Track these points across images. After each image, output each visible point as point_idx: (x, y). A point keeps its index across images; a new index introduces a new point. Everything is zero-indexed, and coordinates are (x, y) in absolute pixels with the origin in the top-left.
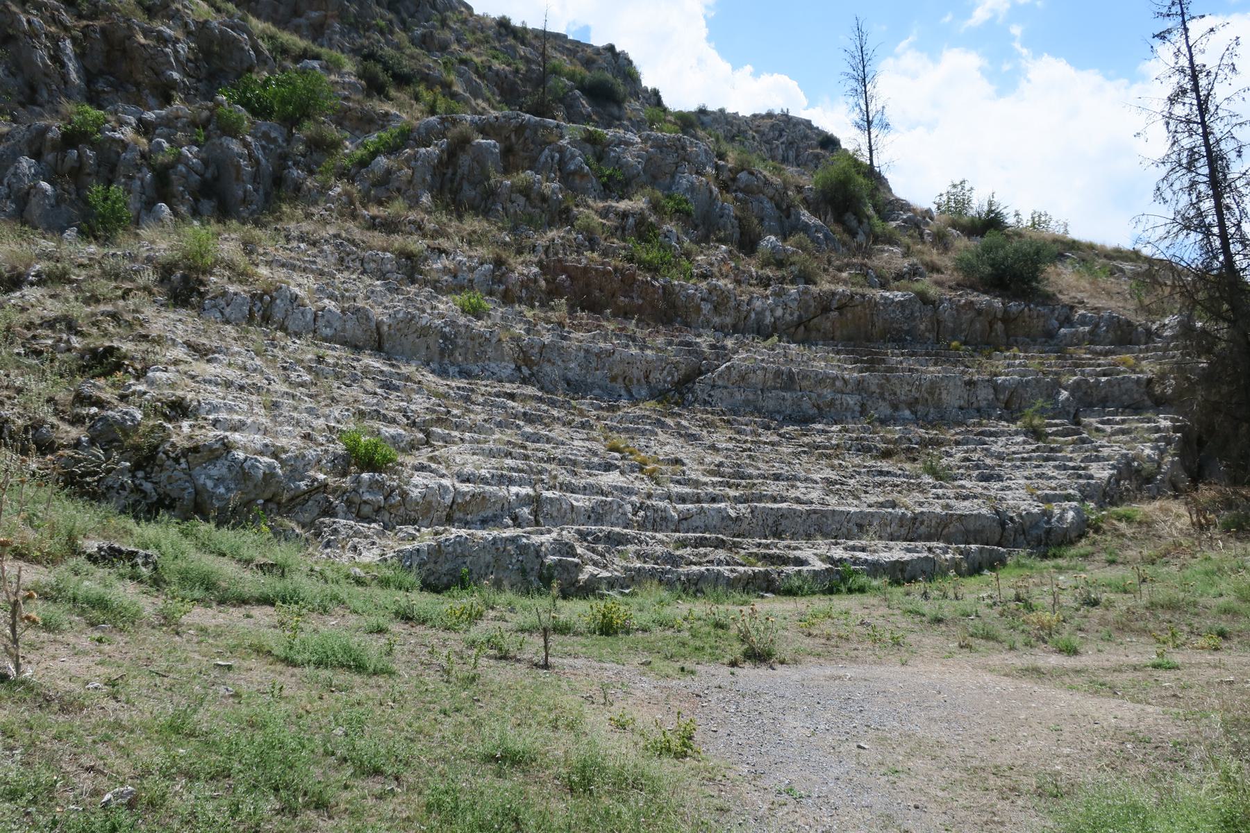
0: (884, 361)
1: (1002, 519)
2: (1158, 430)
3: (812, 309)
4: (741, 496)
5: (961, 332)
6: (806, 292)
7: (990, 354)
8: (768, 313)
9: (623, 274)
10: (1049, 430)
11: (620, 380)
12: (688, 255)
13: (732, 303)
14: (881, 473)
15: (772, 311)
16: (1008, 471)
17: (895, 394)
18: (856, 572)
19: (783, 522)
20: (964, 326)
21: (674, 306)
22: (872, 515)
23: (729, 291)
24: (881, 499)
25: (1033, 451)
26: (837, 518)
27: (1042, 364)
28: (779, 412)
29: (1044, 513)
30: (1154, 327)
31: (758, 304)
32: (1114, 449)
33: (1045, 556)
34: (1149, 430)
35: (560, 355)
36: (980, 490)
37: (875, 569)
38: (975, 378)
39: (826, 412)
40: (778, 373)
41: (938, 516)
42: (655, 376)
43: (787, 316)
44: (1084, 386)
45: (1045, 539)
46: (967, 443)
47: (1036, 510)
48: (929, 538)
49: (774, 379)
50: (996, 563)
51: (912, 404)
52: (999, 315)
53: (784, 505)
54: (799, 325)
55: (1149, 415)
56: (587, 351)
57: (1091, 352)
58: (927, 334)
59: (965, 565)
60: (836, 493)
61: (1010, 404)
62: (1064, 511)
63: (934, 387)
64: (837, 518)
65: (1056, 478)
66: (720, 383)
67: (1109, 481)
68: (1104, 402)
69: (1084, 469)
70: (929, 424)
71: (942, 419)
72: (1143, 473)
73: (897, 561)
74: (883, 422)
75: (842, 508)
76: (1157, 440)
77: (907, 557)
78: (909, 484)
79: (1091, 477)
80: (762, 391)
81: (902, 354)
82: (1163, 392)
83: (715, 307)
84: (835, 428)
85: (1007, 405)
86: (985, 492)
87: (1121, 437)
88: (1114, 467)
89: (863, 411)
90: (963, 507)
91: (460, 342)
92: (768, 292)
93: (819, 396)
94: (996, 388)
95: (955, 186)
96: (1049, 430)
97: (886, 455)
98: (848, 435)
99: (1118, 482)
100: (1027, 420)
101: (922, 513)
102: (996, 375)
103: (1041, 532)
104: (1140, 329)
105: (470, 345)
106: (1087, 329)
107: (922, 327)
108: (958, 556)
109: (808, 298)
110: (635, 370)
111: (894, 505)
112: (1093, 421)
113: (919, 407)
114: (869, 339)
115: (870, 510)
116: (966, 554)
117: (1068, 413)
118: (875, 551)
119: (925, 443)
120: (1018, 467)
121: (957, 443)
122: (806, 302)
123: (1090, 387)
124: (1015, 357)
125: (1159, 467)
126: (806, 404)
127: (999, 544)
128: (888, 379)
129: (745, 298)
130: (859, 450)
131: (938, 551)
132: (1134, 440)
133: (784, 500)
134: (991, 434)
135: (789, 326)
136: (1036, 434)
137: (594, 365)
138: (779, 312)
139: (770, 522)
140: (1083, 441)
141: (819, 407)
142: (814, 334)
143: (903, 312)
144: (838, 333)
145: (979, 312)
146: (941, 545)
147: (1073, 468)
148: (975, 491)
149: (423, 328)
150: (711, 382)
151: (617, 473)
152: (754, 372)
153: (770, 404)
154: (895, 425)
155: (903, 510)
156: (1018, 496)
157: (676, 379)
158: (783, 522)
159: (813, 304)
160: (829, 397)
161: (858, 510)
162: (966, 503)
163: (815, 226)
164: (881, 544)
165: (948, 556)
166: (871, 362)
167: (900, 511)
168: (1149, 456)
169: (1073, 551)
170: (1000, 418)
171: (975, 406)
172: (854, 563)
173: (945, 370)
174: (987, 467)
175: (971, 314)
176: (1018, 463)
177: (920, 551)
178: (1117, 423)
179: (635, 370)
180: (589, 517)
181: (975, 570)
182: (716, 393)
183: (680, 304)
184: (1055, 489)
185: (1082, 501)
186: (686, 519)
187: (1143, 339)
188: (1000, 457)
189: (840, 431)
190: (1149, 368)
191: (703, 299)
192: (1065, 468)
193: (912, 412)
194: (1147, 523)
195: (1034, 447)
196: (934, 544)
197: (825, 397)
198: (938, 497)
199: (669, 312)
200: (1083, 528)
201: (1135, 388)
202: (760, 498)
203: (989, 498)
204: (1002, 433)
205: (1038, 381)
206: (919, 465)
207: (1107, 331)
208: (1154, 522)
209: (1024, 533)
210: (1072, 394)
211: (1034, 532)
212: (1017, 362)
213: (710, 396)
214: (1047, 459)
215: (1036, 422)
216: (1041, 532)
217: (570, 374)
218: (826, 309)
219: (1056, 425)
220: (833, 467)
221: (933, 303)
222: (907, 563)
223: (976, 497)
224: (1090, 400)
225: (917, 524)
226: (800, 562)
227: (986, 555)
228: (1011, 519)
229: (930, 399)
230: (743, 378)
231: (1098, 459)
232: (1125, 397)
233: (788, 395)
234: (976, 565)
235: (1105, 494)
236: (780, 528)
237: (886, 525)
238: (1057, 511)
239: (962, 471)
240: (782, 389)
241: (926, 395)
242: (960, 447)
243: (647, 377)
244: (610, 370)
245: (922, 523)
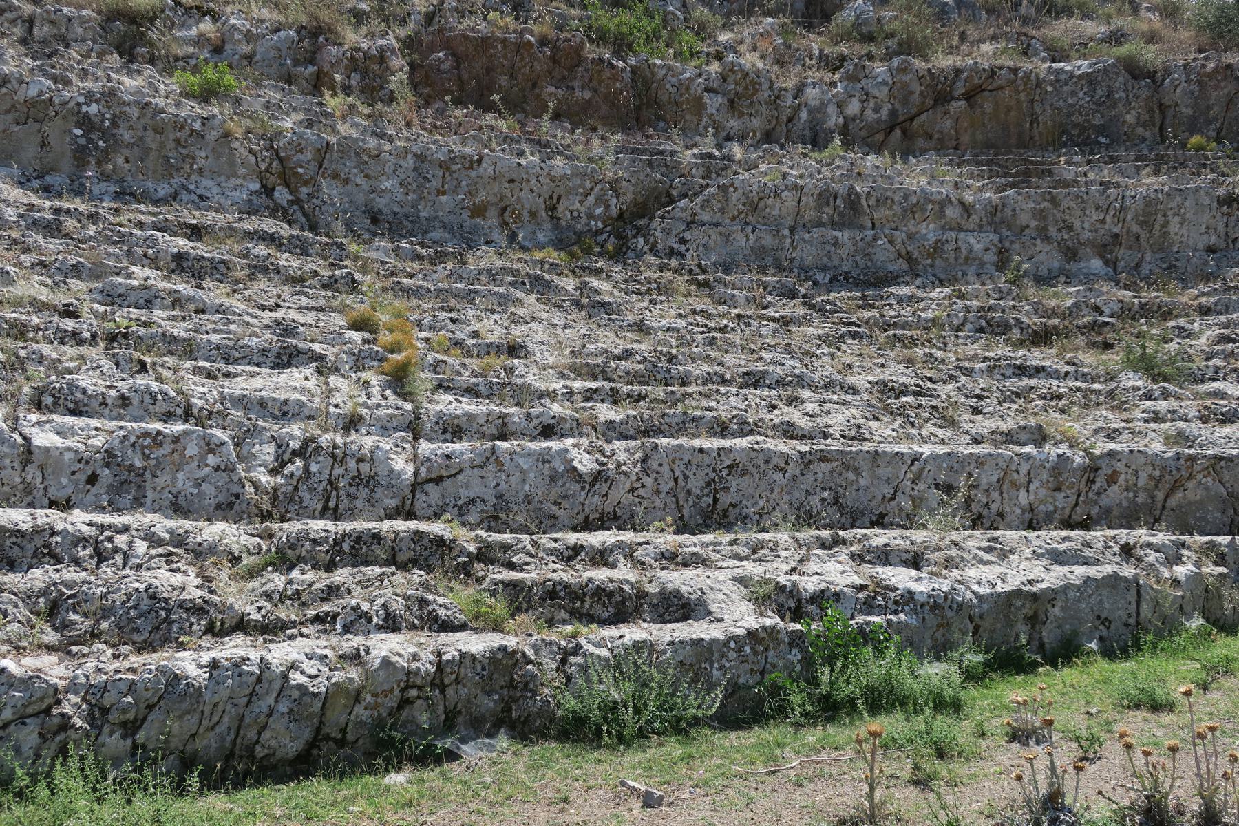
3: (916, 98)
4: (626, 421)
5: (1209, 122)
8: (832, 109)
9: (555, 49)
11: (492, 214)
12: (701, 31)
13: (764, 94)
14: (1021, 370)
15: (840, 106)
17: (1070, 228)
18: (866, 636)
21: (653, 102)
22: (979, 461)
26: (884, 472)
28: (824, 269)
31: (812, 94)
35: (361, 164)
39: (920, 266)
40: (826, 197)
41: (1154, 460)
42: (569, 207)
43: (869, 112)
48: (1129, 520)
49: (818, 208)
51: (1106, 248)
53: (743, 442)
54: (891, 129)
56: (420, 158)
58: (1140, 131)
63: (1151, 208)
64: (884, 472)
66: (706, 217)
70: (1134, 277)
71: (1174, 270)
73: (1017, 593)
75: (903, 448)
77: (1052, 577)
78: (1087, 393)
80: (792, 230)
83: (731, 102)
89: (1002, 264)
91: (127, 135)
92: (837, 76)
93: (911, 236)
97: (1041, 338)
98: (961, 303)
101: (1111, 454)
105: (152, 141)
107: (1130, 118)
108: (1210, 569)
111: (1040, 437)
113: (1122, 252)
114: (1025, 143)
115: (976, 450)
118: (949, 563)
119: (1128, 314)
121: (1204, 311)
122: (905, 85)
126: (883, 254)
128: (1054, 201)
129: (791, 83)
130: (982, 330)
133: (746, 429)
135: (872, 130)
137: (436, 183)
138: (853, 107)
139: (696, 483)
141: (909, 258)
142: (920, 142)
144: (965, 139)
146: (1161, 538)
149: (31, 103)
150: (687, 216)
151: (309, 370)
153: (808, 254)
154: (1068, 283)
155: (1064, 448)
157: (614, 211)
158: (734, 483)
159: (917, 88)
160: (932, 238)
161: (940, 450)
164: (975, 540)
165: (1181, 571)
167: (1052, 452)
172: (869, 606)
177: (1100, 555)
179: (525, 195)
180: (93, 479)
183: (665, 98)
186: (438, 480)
189: (949, 297)
193: (1106, 263)
196: (1142, 534)
197: (924, 238)
198: (1157, 418)
199: (642, 108)
202: (684, 426)
206: (1114, 358)
213: (682, 241)
217: (381, 203)
220: (910, 362)
221: (1152, 75)
222: (1051, 596)
225: (1100, 482)
226: (678, 607)
230: (754, 207)
233: (844, 236)
236: (725, 500)
237: (1015, 486)
239: (1218, 362)
240: (833, 225)
241: (1135, 228)
242: (1211, 319)
243: (554, 208)
244: (471, 193)
245: (1112, 479)
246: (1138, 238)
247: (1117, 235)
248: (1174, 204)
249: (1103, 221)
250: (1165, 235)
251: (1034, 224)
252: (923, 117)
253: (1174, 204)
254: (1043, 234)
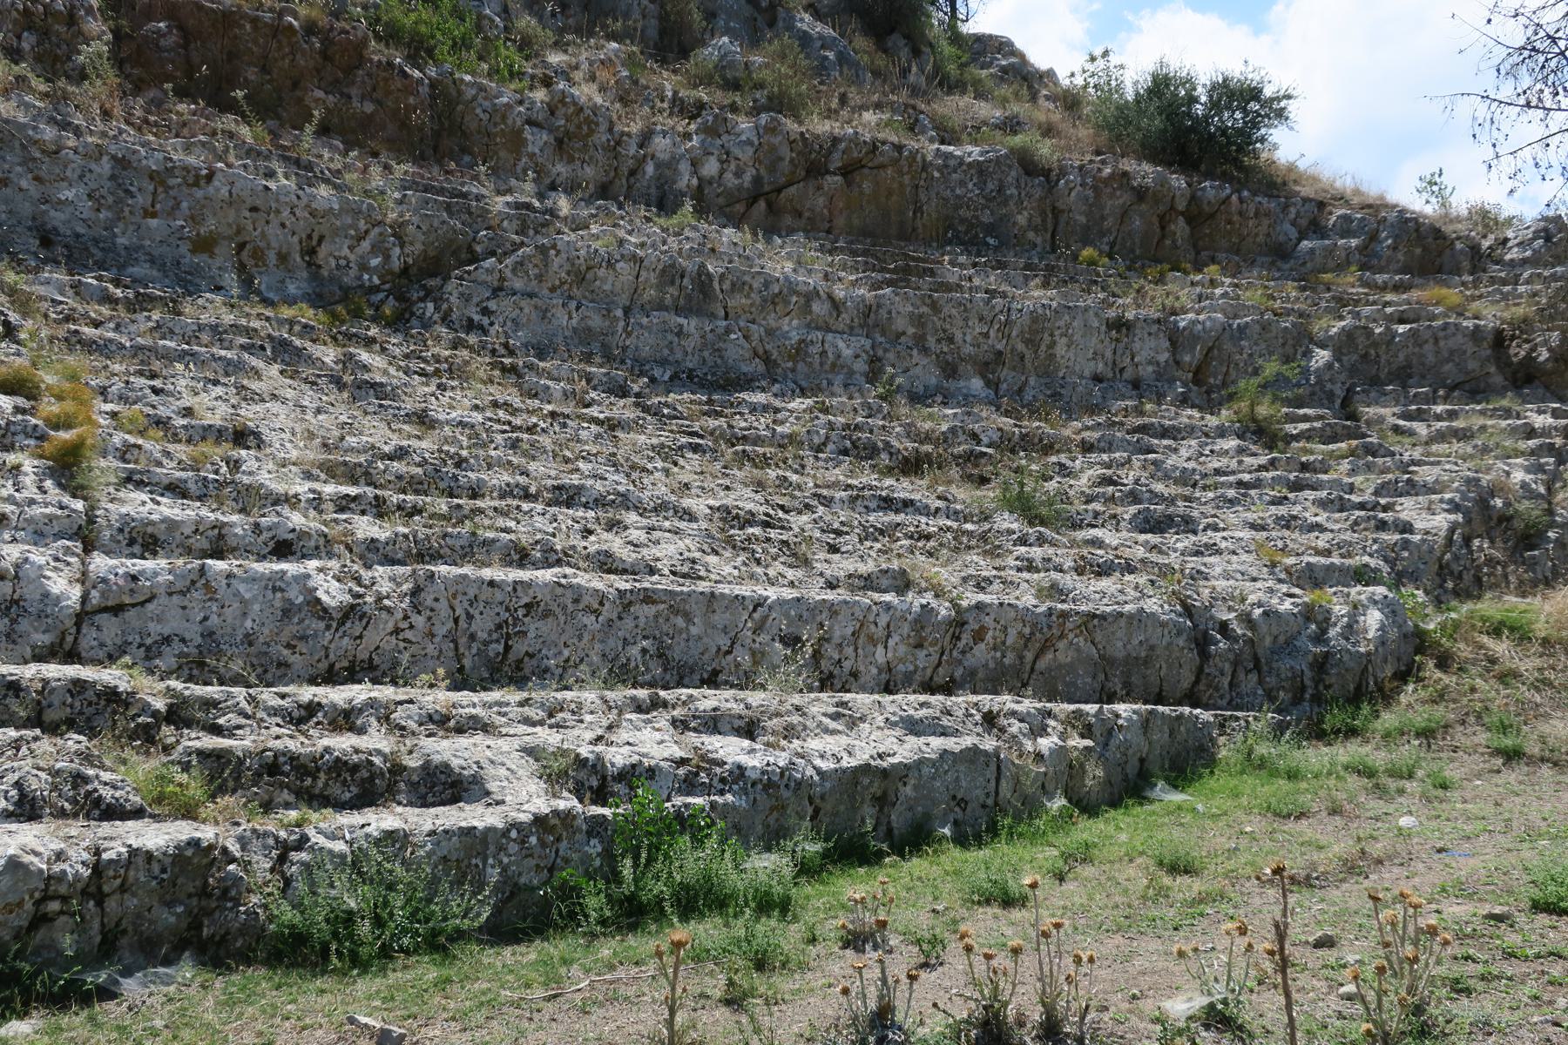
0: (932, 273)
1: (1200, 632)
2: (1531, 432)
5: (1102, 234)
7: (1162, 274)
8: (684, 167)
9: (327, 42)
10: (1292, 429)
12: (526, 45)
13: (602, 137)
14: (887, 503)
17: (951, 340)
18: (683, 822)
19: (533, 626)
20: (1107, 224)
22: (833, 610)
23: (595, 109)
24: (866, 568)
25: (1261, 468)
26: (719, 619)
28: (663, 363)
30: (1486, 244)
31: (661, 144)
32: (1447, 468)
33: (1318, 734)
34: (1513, 430)
36: (1140, 552)
37: (771, 808)
38: (1130, 315)
39: (783, 369)
40: (670, 274)
41: (1024, 615)
43: (728, 176)
44: (1361, 340)
45: (1320, 688)
46: (1110, 448)
47: (1287, 605)
49: (660, 287)
50: (1187, 762)
51: (988, 367)
52: (1181, 205)
53: (546, 575)
54: (753, 200)
55: (1505, 403)
56: (122, 163)
57: (1365, 284)
58: (1031, 235)
59: (1095, 773)
60: (745, 547)
61: (1204, 372)
63: (1038, 325)
64: (719, 619)
66: (518, 284)
67: (1449, 540)
68: (1403, 376)
69: (1385, 509)
71: (1059, 398)
72: (1518, 524)
73: (865, 769)
74: (918, 398)
75: (744, 590)
76: (1533, 453)
77: (904, 750)
79: (1407, 528)
80: (627, 311)
81: (975, 265)
84: (798, 404)
85: (1198, 376)
86: (1154, 557)
87: (1456, 446)
88: (1455, 507)
90: (1098, 594)
93: (770, 332)
94: (1176, 339)
96: (1292, 429)
97: (911, 466)
99: (1467, 541)
100: (1244, 405)
101: (980, 607)
103: (1303, 665)
104: (1459, 246)
106: (1354, 242)
107: (1022, 219)
109: (776, 140)
110: (273, 231)
112: (1388, 413)
113: (1005, 373)
115: (830, 596)
116: (1102, 732)
117: (1331, 396)
118: (789, 732)
121: (1087, 448)
122: (773, 148)
123: (1375, 345)
126: (736, 351)
128: (935, 307)
129: (635, 128)
130: (845, 452)
132: (1485, 450)
133: (552, 558)
134: (1165, 433)
136: (1261, 433)
137: (141, 200)
138: (711, 168)
139: (482, 625)
140: (1372, 451)
141: (767, 359)
142: (788, 220)
143: (982, 185)
144: (840, 222)
145: (1141, 194)
146: (1027, 705)
148: (1127, 553)
150: (493, 280)
153: (645, 343)
155: (928, 597)
156: (1239, 572)
157: (396, 264)
158: (533, 626)
160: (795, 337)
161: (789, 594)
162: (1105, 584)
163: (821, 37)
164: (821, 704)
165: (1045, 744)
166: (906, 270)
167: (914, 600)
168: (1524, 485)
170: (1184, 401)
171: (1127, 375)
172: (689, 785)
173: (1065, 296)
174: (1156, 497)
175: (1124, 198)
176: (1231, 493)
177: (959, 726)
178: (1439, 418)
181: (1130, 787)
182: (503, 306)
183: (473, 126)
184: (1327, 553)
185: (1396, 585)
187: (1466, 264)
188: (1185, 478)
189: (810, 410)
191: (530, 122)
193: (988, 384)
195: (1263, 460)
196: (1006, 701)
197: (786, 336)
199: (443, 134)
200: (1412, 653)
201: (1470, 348)
203: (1165, 571)
204: (1190, 431)
205: (1265, 327)
206: (990, 494)
207: (1395, 248)
210: (1338, 355)
211: (1285, 665)
212: (1218, 291)
213: (485, 312)
214: (1297, 486)
215: (1263, 410)
216: (1303, 665)
217: (57, 218)
218: (815, 170)
219: (1306, 418)
220: (760, 485)
221: (1047, 173)
223: (1129, 568)
224: (1371, 369)
225: (966, 639)
226: (445, 786)
227: (1160, 736)
228: (1224, 627)
229: (1028, 355)
231: (1412, 488)
232: (1448, 367)
233: (691, 324)
234: (1132, 769)
235: (1443, 570)
236: (520, 647)
238: (1340, 609)
240: (678, 311)
241: (1020, 347)
242: (1093, 457)
243: (312, 252)
245: (979, 636)
246: (1022, 358)
247: (1000, 353)
248: (1062, 323)
249: (986, 336)
250: (1052, 357)
251: (911, 331)
252: (792, 190)
253: (1062, 323)
254: (920, 343)
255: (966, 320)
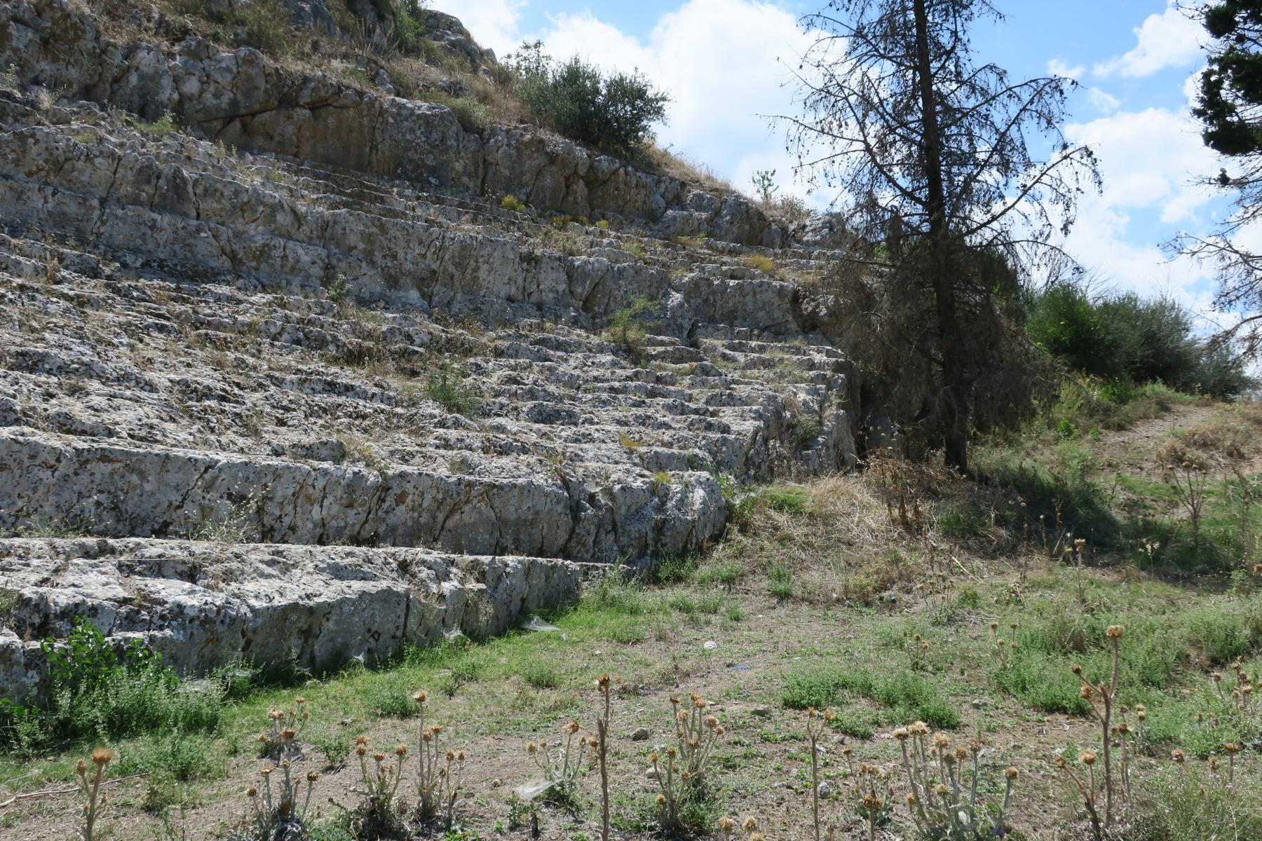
1: (574, 501)
2: (812, 366)
5: (521, 186)
6: (250, 61)
8: (167, 82)
10: (652, 350)
14: (331, 387)
15: (177, 81)
16: (588, 408)
17: (394, 257)
22: (276, 473)
23: (82, 17)
25: (628, 378)
26: (173, 477)
27: (644, 250)
28: (136, 251)
29: (653, 490)
30: (792, 227)
31: (145, 59)
32: (756, 387)
33: (655, 580)
36: (533, 438)
37: (206, 641)
38: (538, 252)
39: (243, 267)
41: (439, 484)
43: (208, 96)
44: (704, 290)
45: (658, 546)
47: (639, 483)
49: (137, 184)
50: (557, 601)
51: (424, 282)
52: (582, 171)
55: (797, 343)
57: (710, 247)
58: (465, 180)
59: (487, 610)
61: (591, 302)
62: (687, 487)
63: (466, 254)
64: (173, 477)
65: (668, 427)
68: (731, 318)
69: (713, 414)
70: (444, 313)
71: (479, 313)
72: (799, 431)
75: (198, 454)
77: (329, 591)
78: (391, 415)
79: (726, 429)
80: (103, 202)
81: (418, 198)
82: (814, 312)
83: (45, 42)
84: (259, 298)
85: (587, 305)
86: (544, 442)
88: (759, 416)
90: (498, 469)
92: (177, 48)
93: (237, 235)
94: (572, 274)
95: (527, 47)
96: (652, 350)
97: (354, 358)
99: (766, 441)
100: (619, 329)
101: (402, 475)
102: (572, 254)
103: (647, 528)
104: (774, 227)
106: (704, 215)
107: (459, 166)
108: (473, 585)
111: (339, 453)
112: (719, 344)
114: (363, 166)
115: (275, 461)
116: (492, 578)
117: (681, 327)
118: (228, 576)
120: (605, 403)
121: (499, 353)
122: (249, 79)
123: (713, 293)
124: (602, 234)
125: (820, 423)
126: (205, 247)
127: (566, 553)
128: (382, 228)
129: (122, 40)
130: (298, 342)
131: (424, 573)
132: (782, 376)
134: (559, 346)
136: (629, 352)
138: (191, 86)
140: (706, 372)
141: (233, 257)
143: (428, 134)
144: (306, 148)
145: (552, 158)
146: (435, 556)
147: (696, 412)
148: (523, 438)
152: (89, 158)
153: (120, 233)
154: (386, 309)
156: (606, 457)
159: (261, 83)
160: (260, 240)
161: (238, 458)
162: (505, 461)
164: (259, 553)
165: (447, 587)
167: (348, 469)
168: (805, 403)
169: (704, 570)
170: (575, 323)
171: (534, 299)
172: (131, 622)
173: (489, 231)
174: (549, 396)
175: (540, 160)
176: (605, 396)
177: (379, 571)
178: (753, 350)
184: (670, 445)
187: (778, 241)
188: (572, 382)
189: (270, 304)
190: (792, 278)
192: (683, 411)
193: (423, 295)
194: (821, 518)
195: (629, 372)
200: (725, 521)
201: (776, 301)
203: (551, 453)
204: (578, 346)
205: (638, 272)
206: (419, 385)
208: (833, 515)
209: (614, 529)
210: (687, 298)
211: (635, 528)
212: (605, 241)
214: (652, 394)
215: (632, 335)
219: (662, 343)
220: (219, 365)
221: (480, 131)
222: (327, 610)
223: (524, 450)
224: (711, 311)
225: (390, 501)
227: (538, 581)
228: (592, 498)
229: (457, 275)
231: (732, 400)
232: (761, 314)
233: (164, 220)
234: (515, 606)
235: (748, 462)
238: (676, 487)
240: (152, 207)
241: (451, 268)
242: (503, 361)
245: (400, 499)
246: (452, 277)
247: (434, 272)
249: (424, 256)
251: (361, 246)
252: (266, 116)
254: (368, 256)
255: (408, 242)
